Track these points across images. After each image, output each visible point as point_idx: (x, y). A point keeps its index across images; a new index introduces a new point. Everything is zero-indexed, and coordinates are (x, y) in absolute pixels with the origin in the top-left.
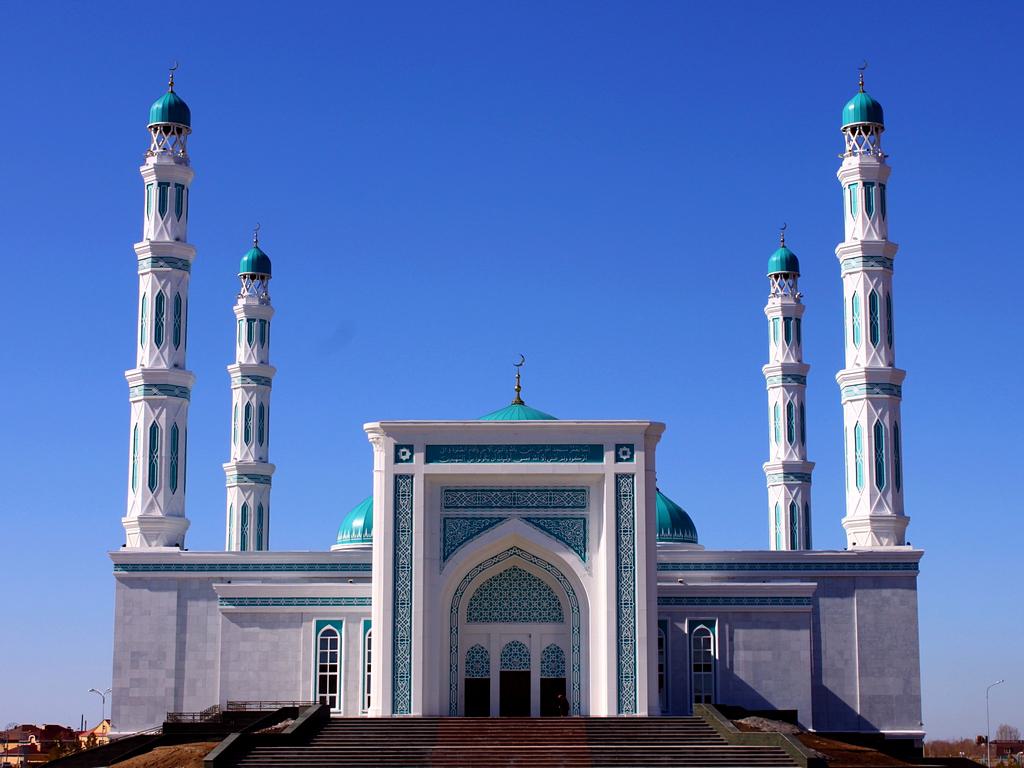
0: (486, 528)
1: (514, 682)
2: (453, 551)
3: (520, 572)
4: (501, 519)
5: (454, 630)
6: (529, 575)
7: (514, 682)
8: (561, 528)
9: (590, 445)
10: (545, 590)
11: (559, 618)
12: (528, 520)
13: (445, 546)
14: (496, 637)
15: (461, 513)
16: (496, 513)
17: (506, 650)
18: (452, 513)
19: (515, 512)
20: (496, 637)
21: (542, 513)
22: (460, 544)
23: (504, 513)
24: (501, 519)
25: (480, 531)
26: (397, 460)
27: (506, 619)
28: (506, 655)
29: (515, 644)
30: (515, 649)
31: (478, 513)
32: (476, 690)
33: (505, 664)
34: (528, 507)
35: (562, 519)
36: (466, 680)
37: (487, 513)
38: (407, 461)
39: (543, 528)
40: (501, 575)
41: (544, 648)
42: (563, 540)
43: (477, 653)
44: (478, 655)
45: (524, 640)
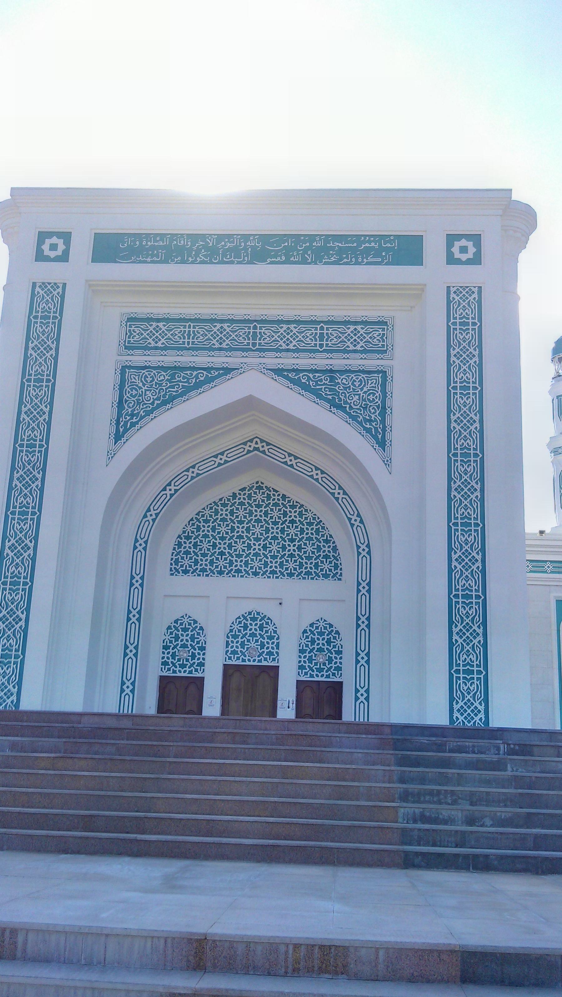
0: (198, 385)
1: (251, 684)
2: (133, 425)
3: (269, 492)
4: (227, 370)
5: (137, 582)
6: (284, 497)
7: (251, 684)
8: (340, 389)
9: (398, 237)
10: (310, 524)
11: (322, 562)
12: (279, 372)
13: (119, 415)
14: (216, 604)
15: (154, 359)
16: (219, 360)
17: (236, 627)
18: (138, 359)
19: (253, 360)
20: (216, 604)
21: (304, 362)
22: (148, 413)
23: (232, 360)
24: (227, 370)
25: (187, 390)
26: (40, 257)
27: (238, 571)
28: (235, 636)
29: (253, 616)
30: (253, 626)
31: (186, 359)
32: (179, 693)
33: (234, 652)
34: (345, 351)
35: (342, 372)
36: (162, 678)
37: (202, 360)
38: (257, 437)
39: (306, 387)
40: (234, 496)
41: (305, 625)
42: (343, 409)
43: (185, 630)
44: (185, 634)
45: (269, 609)
